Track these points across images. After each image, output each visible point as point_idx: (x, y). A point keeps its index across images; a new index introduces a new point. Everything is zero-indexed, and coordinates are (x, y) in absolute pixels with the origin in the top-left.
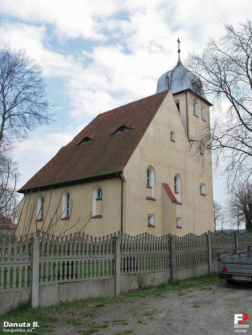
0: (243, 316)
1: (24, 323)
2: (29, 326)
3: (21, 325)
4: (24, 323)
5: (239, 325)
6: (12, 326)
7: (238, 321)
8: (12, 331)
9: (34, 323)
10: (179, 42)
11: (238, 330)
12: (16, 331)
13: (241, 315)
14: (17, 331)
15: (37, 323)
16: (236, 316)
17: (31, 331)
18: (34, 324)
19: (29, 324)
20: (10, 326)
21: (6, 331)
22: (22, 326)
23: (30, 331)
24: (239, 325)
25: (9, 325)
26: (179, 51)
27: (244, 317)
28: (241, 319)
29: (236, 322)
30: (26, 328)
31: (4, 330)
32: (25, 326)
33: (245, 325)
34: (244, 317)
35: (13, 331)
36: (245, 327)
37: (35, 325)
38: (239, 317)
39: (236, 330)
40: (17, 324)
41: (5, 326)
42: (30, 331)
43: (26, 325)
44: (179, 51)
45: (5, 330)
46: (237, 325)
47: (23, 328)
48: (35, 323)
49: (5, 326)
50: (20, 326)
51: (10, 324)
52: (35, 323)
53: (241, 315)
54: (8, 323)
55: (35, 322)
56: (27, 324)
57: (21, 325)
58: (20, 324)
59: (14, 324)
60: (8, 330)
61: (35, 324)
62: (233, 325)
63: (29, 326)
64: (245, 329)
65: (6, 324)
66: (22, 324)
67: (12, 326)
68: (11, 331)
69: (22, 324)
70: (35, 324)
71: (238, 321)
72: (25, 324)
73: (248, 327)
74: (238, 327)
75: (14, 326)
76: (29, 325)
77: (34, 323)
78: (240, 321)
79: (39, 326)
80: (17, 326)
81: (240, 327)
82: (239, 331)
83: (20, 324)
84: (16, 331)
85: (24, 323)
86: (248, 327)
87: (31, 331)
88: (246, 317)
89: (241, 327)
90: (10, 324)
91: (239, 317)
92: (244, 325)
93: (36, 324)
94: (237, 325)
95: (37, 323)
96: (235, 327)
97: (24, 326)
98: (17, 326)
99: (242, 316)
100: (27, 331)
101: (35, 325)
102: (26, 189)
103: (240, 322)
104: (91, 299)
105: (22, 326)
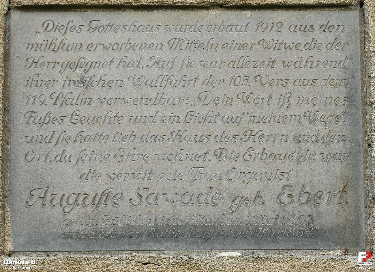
0: (367, 254)
2: (28, 264)
13: (365, 253)
16: (360, 254)
22: (21, 263)
27: (368, 255)
28: (365, 257)
34: (368, 255)
37: (33, 263)
52: (33, 261)
53: (365, 253)
61: (33, 262)
67: (11, 264)
72: (24, 261)
75: (13, 264)
78: (363, 259)
82: (363, 268)
88: (370, 254)
98: (16, 263)
103: (364, 260)
104: (312, 6)
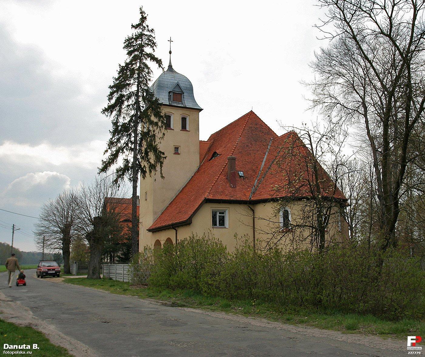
1: (24, 345)
2: (29, 348)
3: (21, 347)
4: (24, 345)
5: (412, 347)
6: (12, 348)
7: (411, 343)
8: (12, 353)
9: (34, 345)
10: (170, 41)
11: (411, 352)
12: (16, 353)
14: (17, 353)
15: (37, 345)
16: (409, 338)
17: (30, 353)
18: (34, 346)
19: (29, 346)
20: (10, 348)
21: (6, 353)
23: (30, 353)
24: (412, 347)
25: (9, 347)
26: (170, 53)
28: (414, 341)
29: (409, 344)
30: (26, 350)
31: (4, 352)
32: (25, 348)
33: (419, 347)
35: (13, 353)
36: (418, 349)
38: (412, 339)
39: (409, 352)
40: (17, 346)
41: (5, 348)
42: (30, 353)
43: (26, 347)
44: (170, 53)
45: (5, 352)
46: (410, 347)
47: (22, 350)
48: (35, 345)
49: (5, 348)
50: (20, 348)
51: (10, 346)
52: (35, 345)
53: (414, 337)
54: (8, 345)
55: (35, 344)
56: (27, 346)
57: (21, 347)
58: (19, 346)
59: (14, 346)
60: (8, 352)
61: (35, 346)
62: (407, 346)
63: (29, 348)
64: (418, 351)
65: (6, 346)
66: (22, 346)
67: (12, 348)
68: (11, 353)
69: (22, 346)
70: (35, 346)
71: (411, 343)
72: (25, 346)
73: (421, 349)
74: (411, 349)
75: (14, 348)
76: (29, 347)
77: (34, 345)
79: (38, 348)
80: (17, 348)
81: (413, 349)
82: (412, 353)
83: (19, 346)
84: (16, 353)
85: (24, 345)
86: (421, 349)
87: (30, 353)
89: (414, 349)
90: (10, 346)
91: (412, 339)
92: (417, 347)
93: (36, 346)
94: (410, 347)
95: (37, 345)
96: (408, 349)
97: (24, 348)
98: (17, 348)
99: (415, 338)
100: (27, 354)
101: (35, 347)
102: (154, 227)
103: (413, 345)
105: (22, 348)
